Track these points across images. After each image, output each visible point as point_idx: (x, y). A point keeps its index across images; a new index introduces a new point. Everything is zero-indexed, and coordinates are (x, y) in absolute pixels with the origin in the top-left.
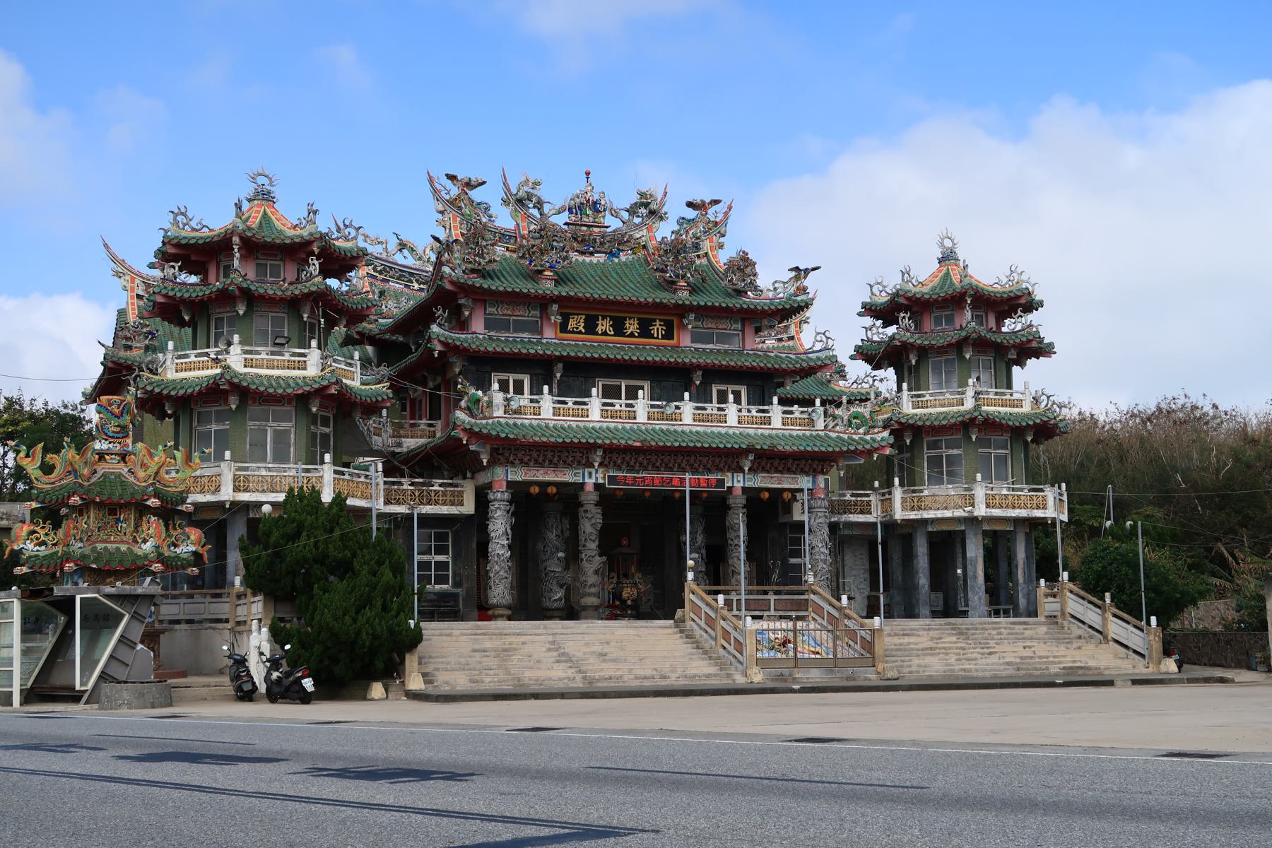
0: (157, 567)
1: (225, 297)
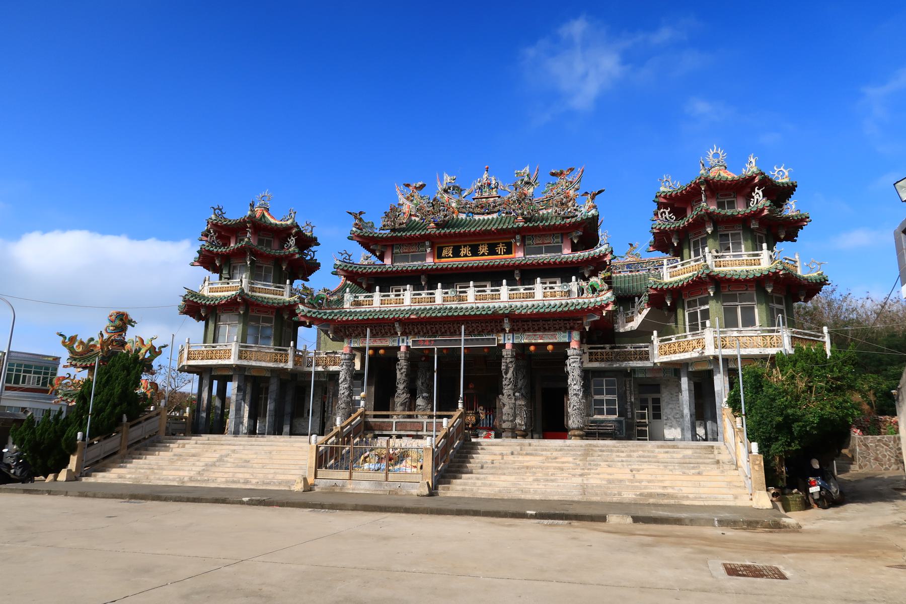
1: (699, 223)
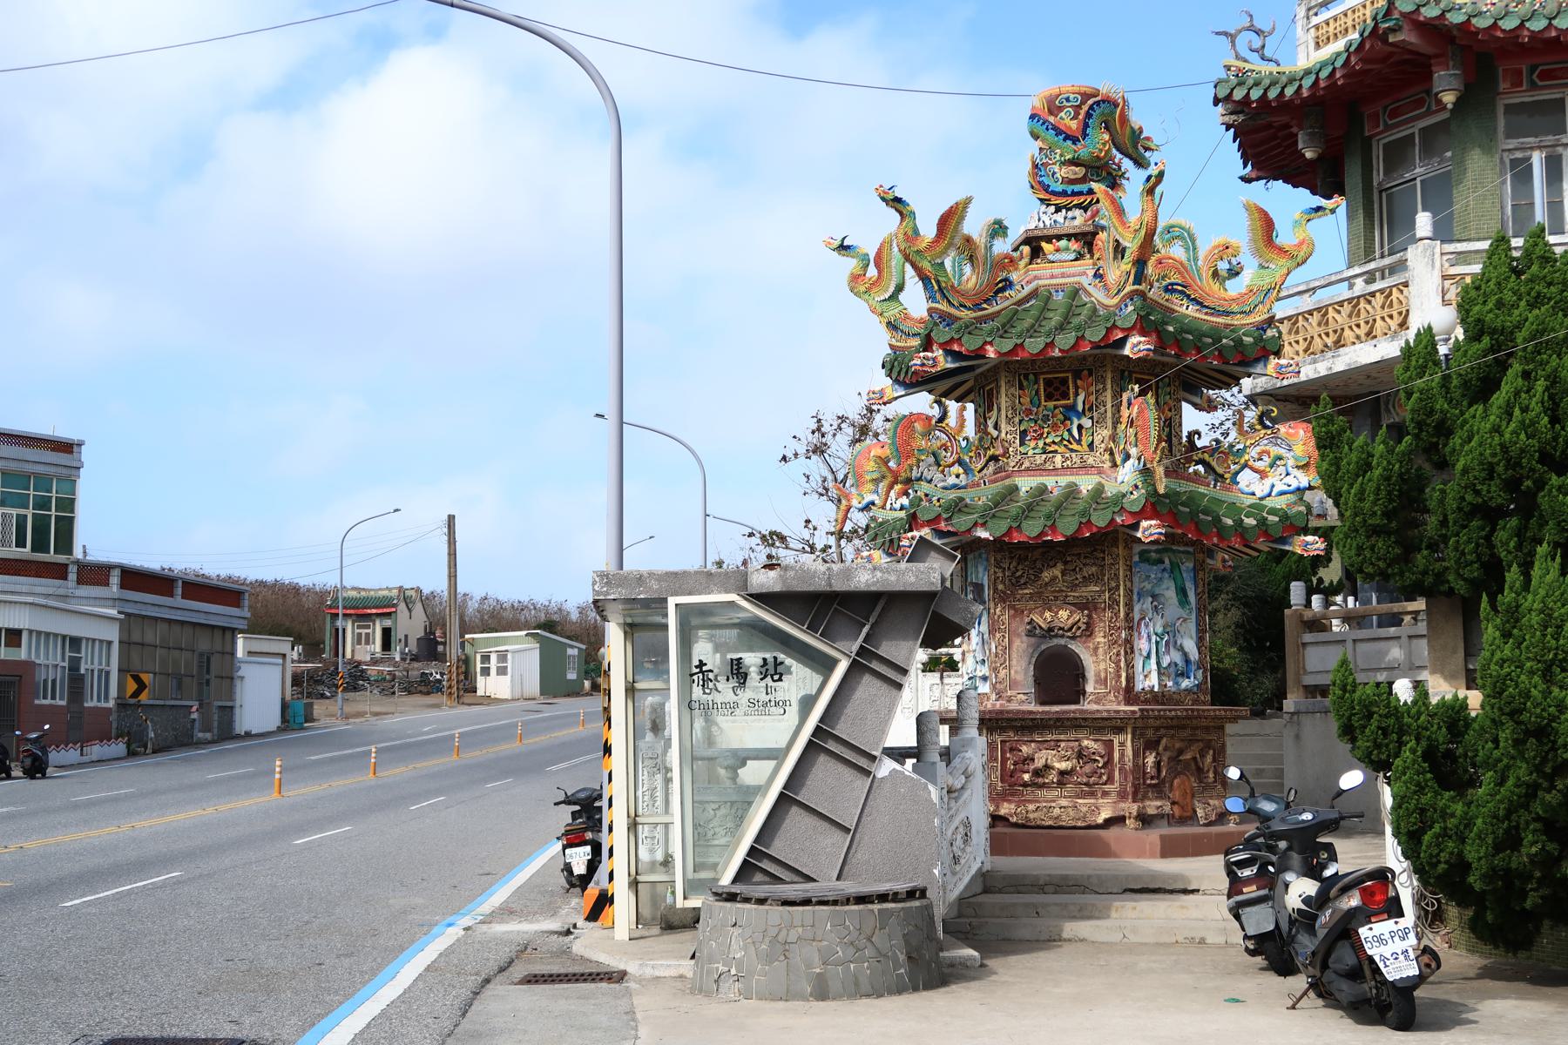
0: (1149, 529)
